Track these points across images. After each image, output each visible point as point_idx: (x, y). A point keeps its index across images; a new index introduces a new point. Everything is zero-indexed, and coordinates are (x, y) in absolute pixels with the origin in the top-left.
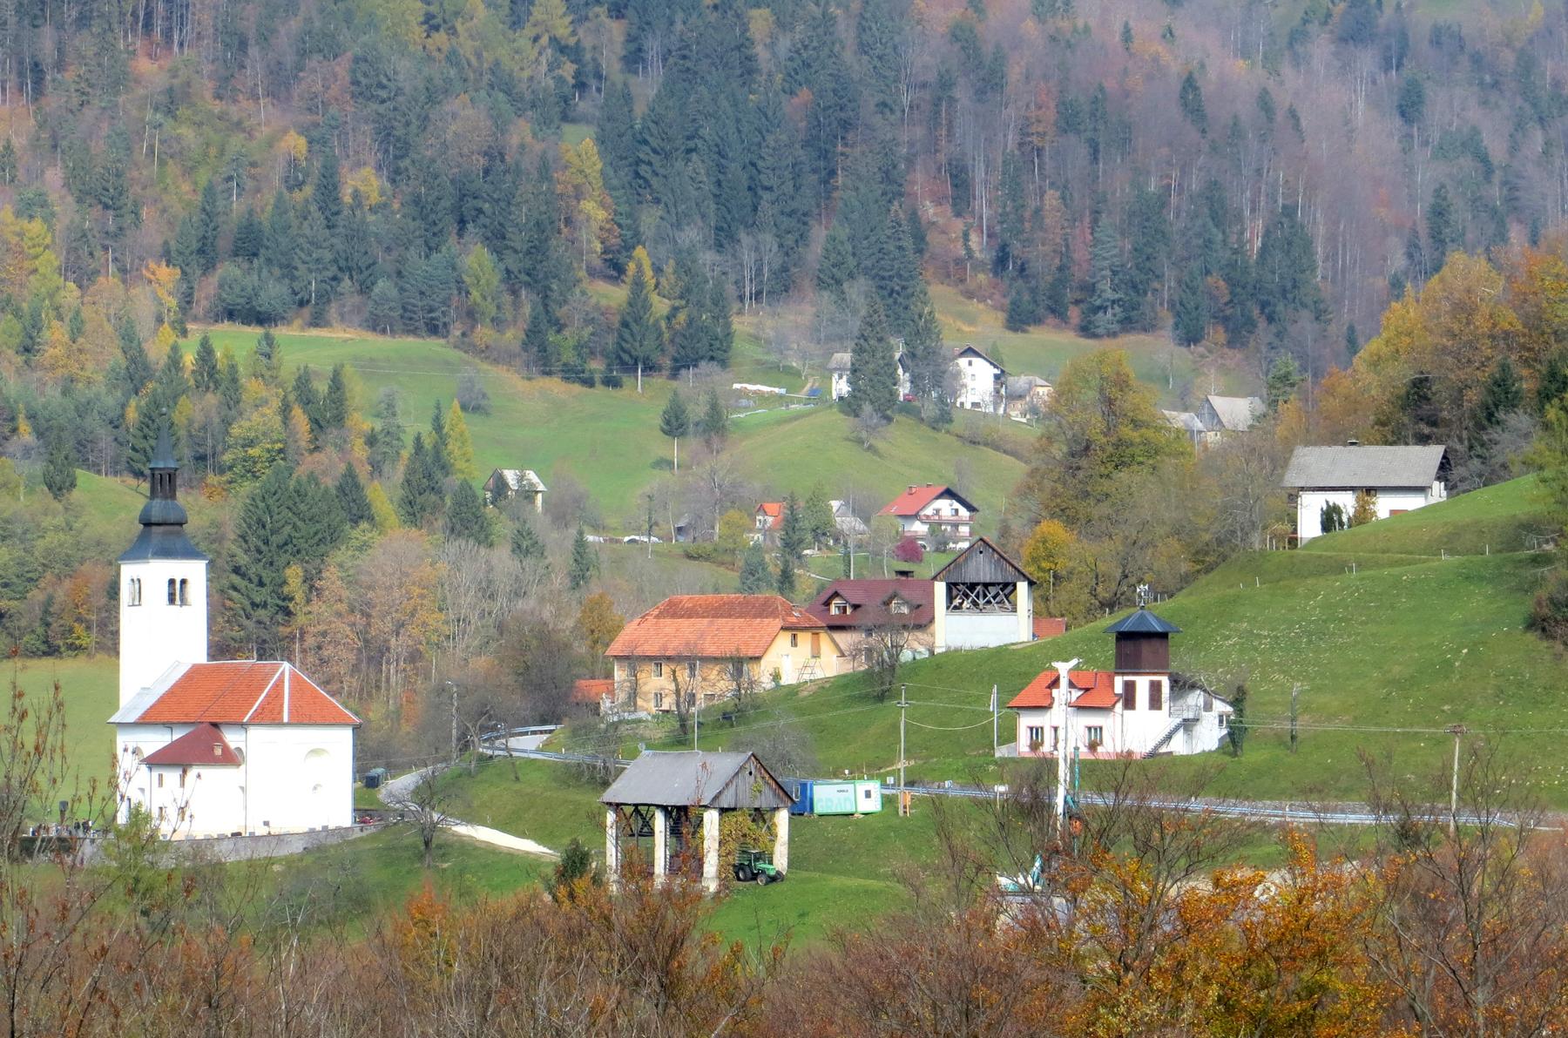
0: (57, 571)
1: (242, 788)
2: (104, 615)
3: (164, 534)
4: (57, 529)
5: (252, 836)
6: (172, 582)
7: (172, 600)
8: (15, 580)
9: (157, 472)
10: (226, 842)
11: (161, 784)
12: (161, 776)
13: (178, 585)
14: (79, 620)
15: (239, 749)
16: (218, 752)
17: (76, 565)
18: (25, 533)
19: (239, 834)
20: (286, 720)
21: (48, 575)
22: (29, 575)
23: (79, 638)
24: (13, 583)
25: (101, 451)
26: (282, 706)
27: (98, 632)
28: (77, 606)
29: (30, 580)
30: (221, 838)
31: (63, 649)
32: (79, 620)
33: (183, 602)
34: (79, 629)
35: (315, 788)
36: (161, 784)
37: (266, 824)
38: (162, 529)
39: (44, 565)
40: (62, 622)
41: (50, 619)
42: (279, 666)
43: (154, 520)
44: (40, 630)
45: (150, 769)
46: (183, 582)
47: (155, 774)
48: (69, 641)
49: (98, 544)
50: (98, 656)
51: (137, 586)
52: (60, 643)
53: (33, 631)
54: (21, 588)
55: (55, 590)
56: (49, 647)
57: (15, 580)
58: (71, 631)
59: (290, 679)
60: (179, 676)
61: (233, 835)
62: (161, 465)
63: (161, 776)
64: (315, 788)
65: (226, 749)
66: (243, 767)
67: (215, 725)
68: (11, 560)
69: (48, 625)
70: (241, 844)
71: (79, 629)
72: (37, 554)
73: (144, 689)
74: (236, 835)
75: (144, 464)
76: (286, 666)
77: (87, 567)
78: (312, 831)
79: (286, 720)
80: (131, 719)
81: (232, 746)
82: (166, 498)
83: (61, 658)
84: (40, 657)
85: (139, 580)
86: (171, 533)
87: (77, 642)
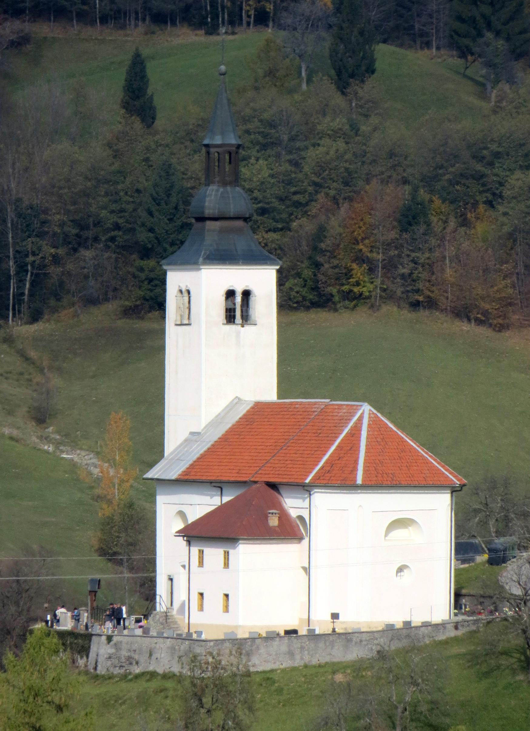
0: (332, 192)
1: (304, 569)
2: (393, 252)
3: (222, 231)
4: (335, 135)
5: (312, 635)
6: (230, 294)
7: (230, 317)
8: (276, 204)
9: (212, 150)
10: (276, 642)
11: (201, 563)
12: (201, 552)
13: (239, 299)
14: (360, 259)
15: (301, 518)
16: (274, 521)
17: (360, 183)
18: (292, 139)
19: (295, 632)
20: (359, 481)
21: (321, 197)
22: (296, 198)
23: (358, 284)
24: (274, 209)
25: (431, 16)
26: (356, 462)
27: (384, 275)
28: (357, 242)
29: (298, 204)
30: (272, 636)
31: (336, 299)
32: (360, 259)
33: (246, 318)
34: (358, 271)
35: (400, 570)
36: (201, 563)
37: (335, 616)
38: (217, 225)
39: (316, 184)
40: (335, 262)
41: (320, 259)
42: (358, 408)
43: (208, 212)
44: (307, 273)
45: (189, 543)
46: (247, 294)
47: (195, 550)
48: (346, 288)
49: (391, 155)
50: (385, 309)
51: (186, 299)
52: (334, 290)
53: (299, 275)
54: (284, 216)
55: (328, 218)
56: (320, 295)
57: (276, 204)
58: (348, 274)
59: (369, 426)
60: (237, 418)
61: (287, 632)
62: (218, 140)
63: (201, 552)
64: (400, 570)
65: (284, 516)
66: (305, 542)
67: (273, 486)
68: (272, 176)
69: (318, 265)
70: (296, 644)
71: (358, 271)
72: (306, 169)
73: (192, 433)
74: (291, 632)
75: (474, 40)
76: (366, 409)
77: (374, 186)
78: (390, 628)
79: (359, 481)
80: (173, 475)
81: (293, 514)
82: (224, 184)
83: (336, 310)
84: (308, 308)
85: (189, 292)
86: (231, 230)
87: (356, 289)
